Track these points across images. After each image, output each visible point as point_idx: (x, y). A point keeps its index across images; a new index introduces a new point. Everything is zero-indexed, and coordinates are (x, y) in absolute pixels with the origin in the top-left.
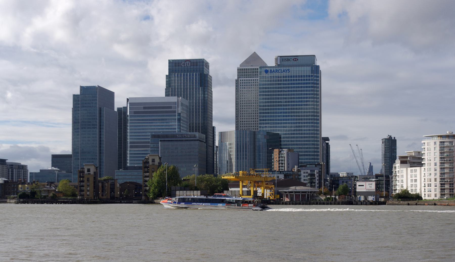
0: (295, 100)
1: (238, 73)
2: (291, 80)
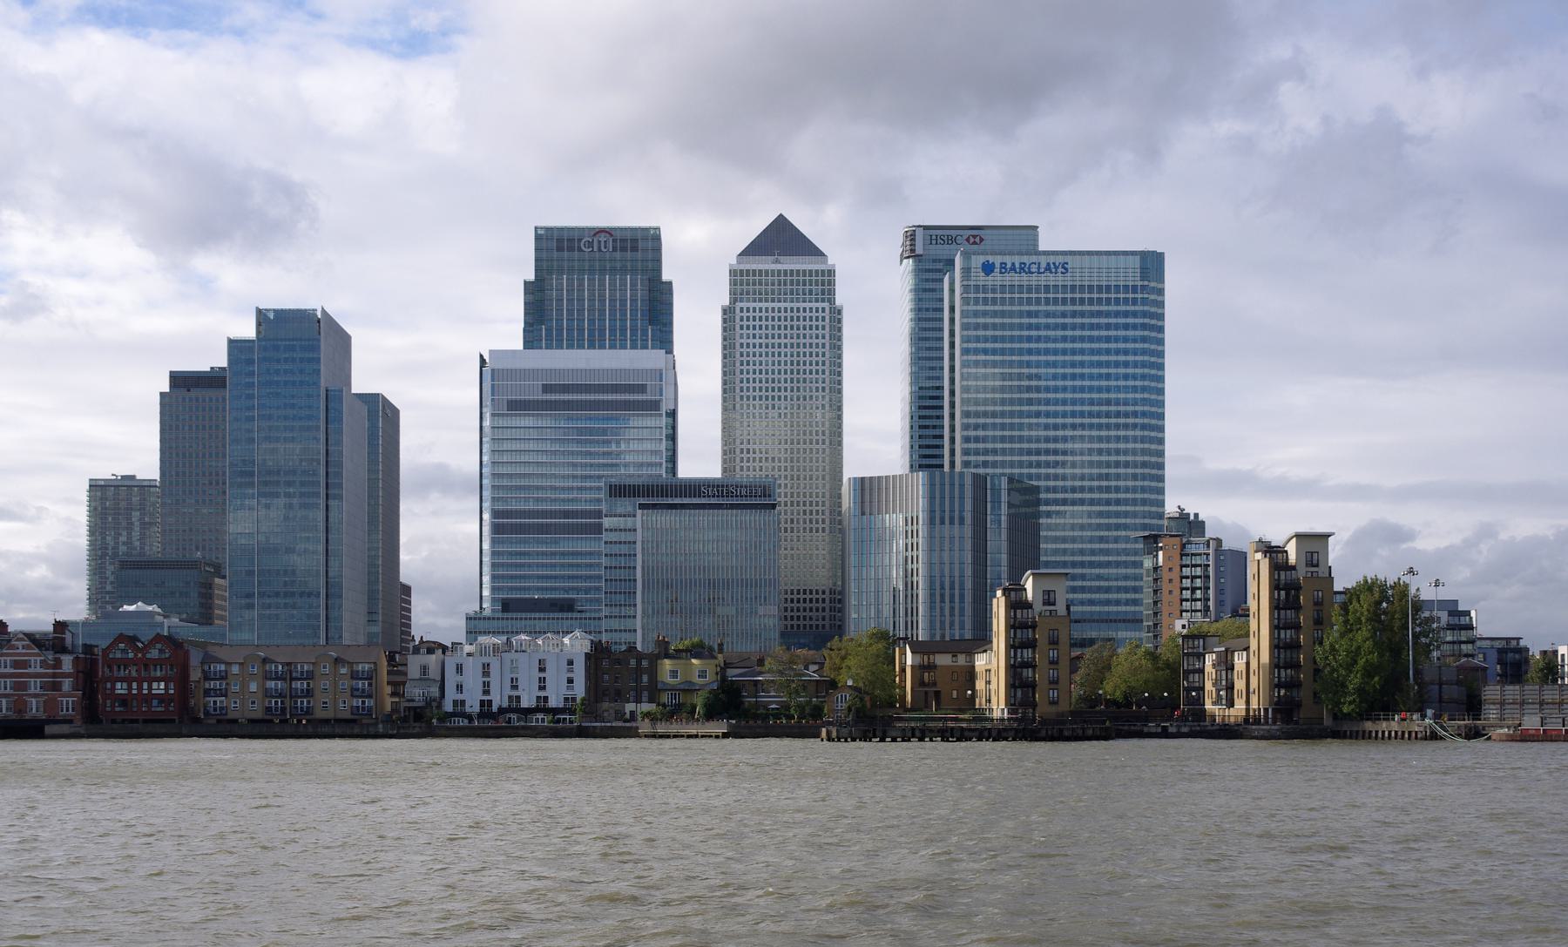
0: (1086, 371)
1: (733, 283)
2: (1073, 301)
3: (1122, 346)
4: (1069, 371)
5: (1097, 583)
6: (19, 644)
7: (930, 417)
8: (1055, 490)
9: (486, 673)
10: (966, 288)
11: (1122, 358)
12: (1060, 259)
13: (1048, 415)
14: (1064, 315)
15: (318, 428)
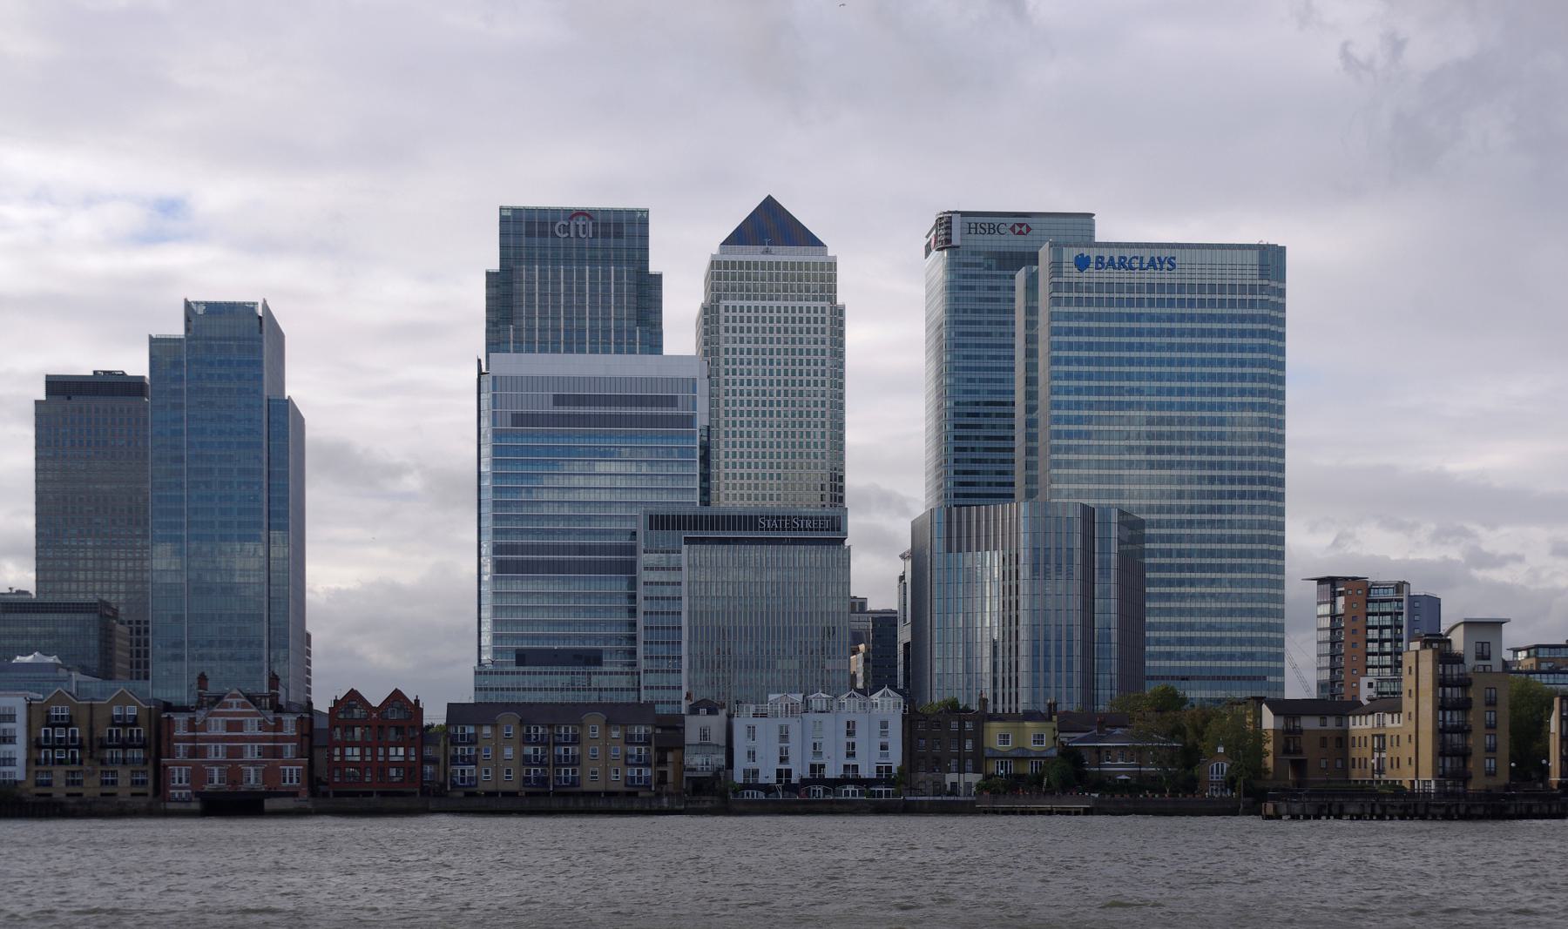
0: (1196, 385)
3: (1237, 355)
4: (1226, 385)
5: (1208, 634)
6: (234, 701)
7: (967, 438)
8: (1159, 524)
9: (784, 737)
10: (1056, 287)
11: (1237, 370)
12: (1167, 253)
14: (1170, 318)
15: (260, 446)
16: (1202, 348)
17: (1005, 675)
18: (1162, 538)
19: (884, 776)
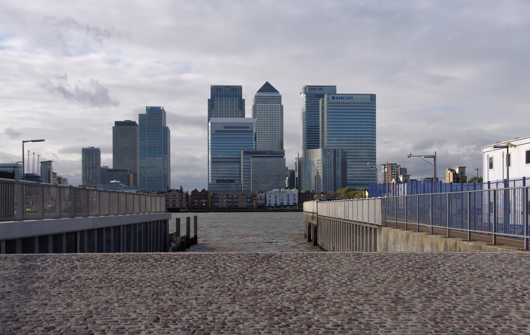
8: (350, 152)
9: (276, 198)
10: (328, 103)
12: (351, 96)
13: (348, 134)
14: (352, 110)
16: (359, 116)
17: (317, 185)
18: (350, 156)
19: (295, 205)
